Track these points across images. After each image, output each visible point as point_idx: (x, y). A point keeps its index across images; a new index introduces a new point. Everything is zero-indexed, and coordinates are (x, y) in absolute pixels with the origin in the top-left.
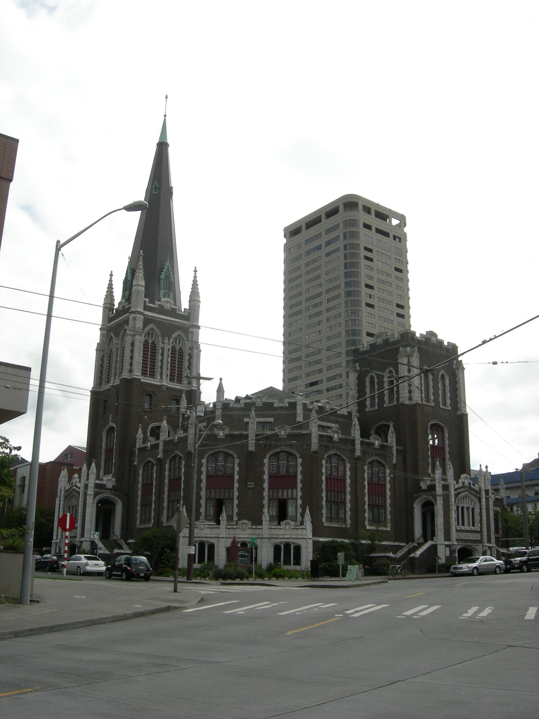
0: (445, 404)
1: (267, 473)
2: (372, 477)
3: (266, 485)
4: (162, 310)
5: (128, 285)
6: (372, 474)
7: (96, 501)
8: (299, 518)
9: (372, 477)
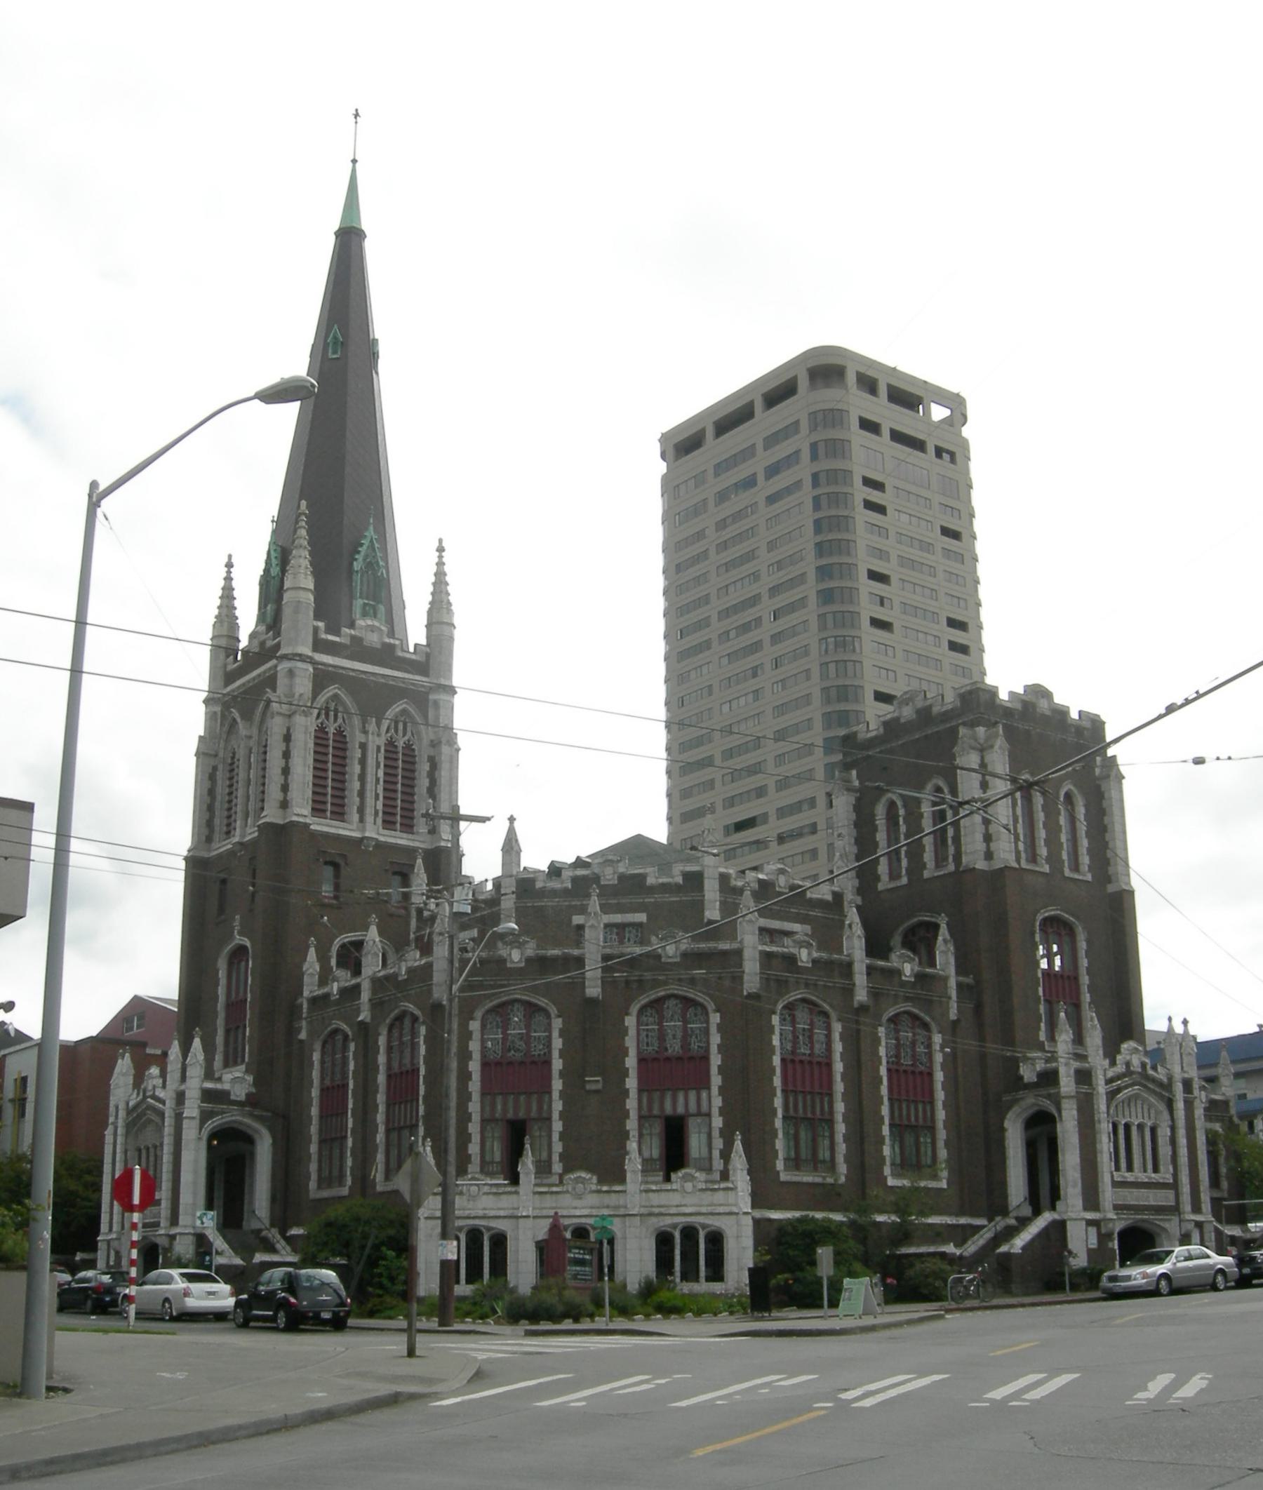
0: (1076, 867)
2: (897, 1056)
3: (632, 1083)
4: (358, 650)
6: (898, 1046)
7: (205, 1134)
8: (718, 1164)
9: (897, 1056)
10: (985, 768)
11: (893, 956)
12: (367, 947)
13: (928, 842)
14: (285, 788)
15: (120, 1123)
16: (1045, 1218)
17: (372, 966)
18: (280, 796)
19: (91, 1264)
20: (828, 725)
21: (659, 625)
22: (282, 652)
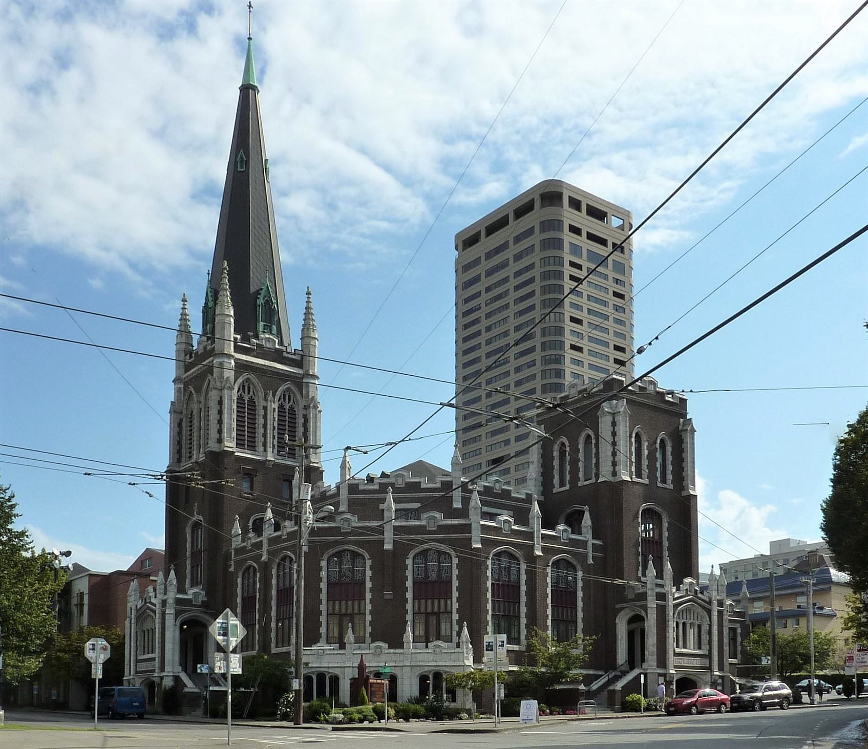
0: (664, 480)
1: (410, 579)
3: (409, 595)
4: (262, 352)
5: (209, 315)
7: (178, 623)
9: (557, 583)
14: (220, 431)
17: (269, 532)
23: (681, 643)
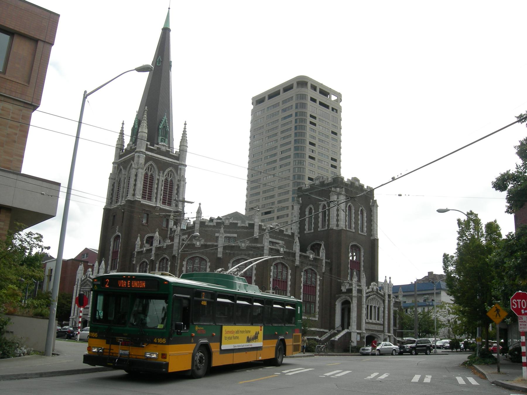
0: (362, 231)
2: (307, 281)
6: (307, 278)
10: (339, 199)
11: (308, 252)
12: (155, 238)
13: (320, 215)
14: (134, 190)
15: (79, 284)
16: (346, 331)
17: (156, 244)
18: (133, 192)
19: (68, 325)
20: (294, 186)
21: (245, 192)
22: (137, 150)
23: (369, 318)
